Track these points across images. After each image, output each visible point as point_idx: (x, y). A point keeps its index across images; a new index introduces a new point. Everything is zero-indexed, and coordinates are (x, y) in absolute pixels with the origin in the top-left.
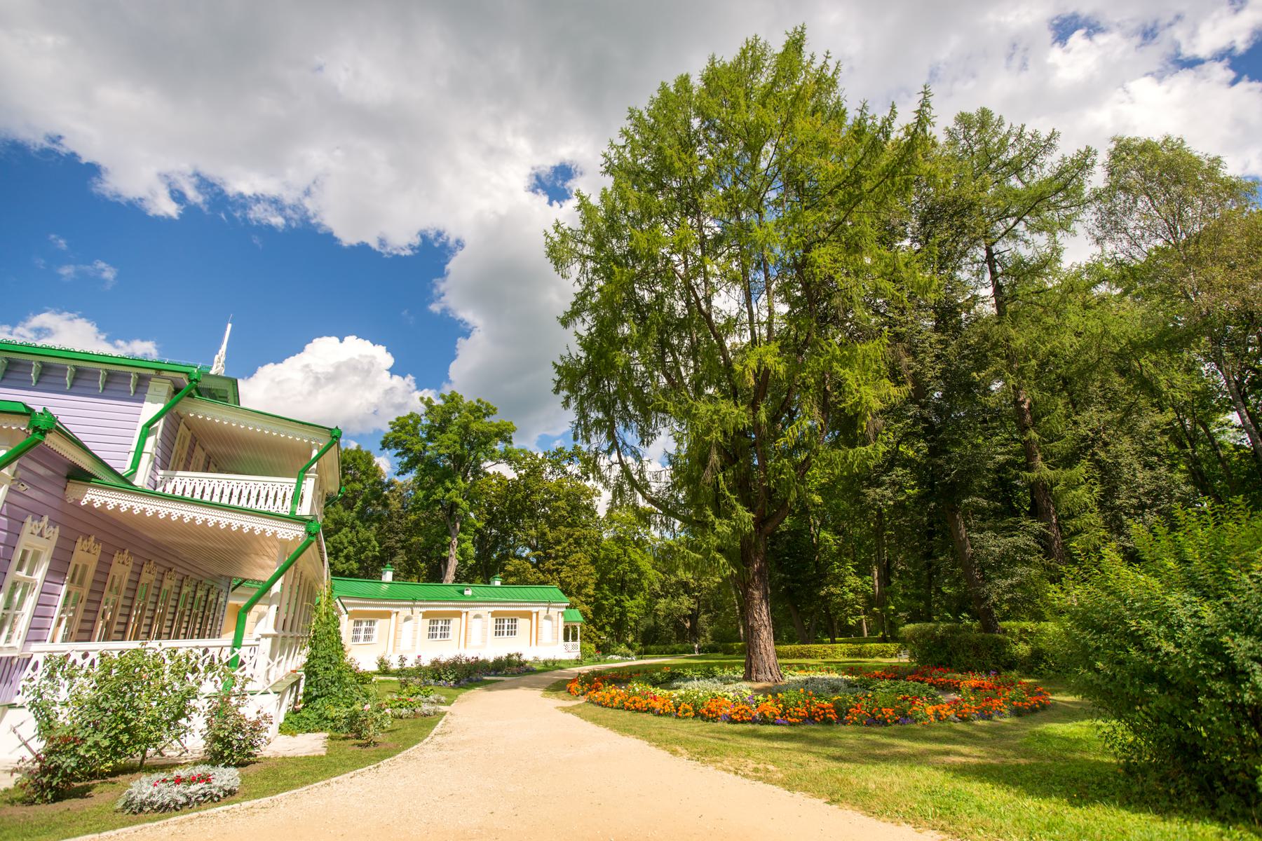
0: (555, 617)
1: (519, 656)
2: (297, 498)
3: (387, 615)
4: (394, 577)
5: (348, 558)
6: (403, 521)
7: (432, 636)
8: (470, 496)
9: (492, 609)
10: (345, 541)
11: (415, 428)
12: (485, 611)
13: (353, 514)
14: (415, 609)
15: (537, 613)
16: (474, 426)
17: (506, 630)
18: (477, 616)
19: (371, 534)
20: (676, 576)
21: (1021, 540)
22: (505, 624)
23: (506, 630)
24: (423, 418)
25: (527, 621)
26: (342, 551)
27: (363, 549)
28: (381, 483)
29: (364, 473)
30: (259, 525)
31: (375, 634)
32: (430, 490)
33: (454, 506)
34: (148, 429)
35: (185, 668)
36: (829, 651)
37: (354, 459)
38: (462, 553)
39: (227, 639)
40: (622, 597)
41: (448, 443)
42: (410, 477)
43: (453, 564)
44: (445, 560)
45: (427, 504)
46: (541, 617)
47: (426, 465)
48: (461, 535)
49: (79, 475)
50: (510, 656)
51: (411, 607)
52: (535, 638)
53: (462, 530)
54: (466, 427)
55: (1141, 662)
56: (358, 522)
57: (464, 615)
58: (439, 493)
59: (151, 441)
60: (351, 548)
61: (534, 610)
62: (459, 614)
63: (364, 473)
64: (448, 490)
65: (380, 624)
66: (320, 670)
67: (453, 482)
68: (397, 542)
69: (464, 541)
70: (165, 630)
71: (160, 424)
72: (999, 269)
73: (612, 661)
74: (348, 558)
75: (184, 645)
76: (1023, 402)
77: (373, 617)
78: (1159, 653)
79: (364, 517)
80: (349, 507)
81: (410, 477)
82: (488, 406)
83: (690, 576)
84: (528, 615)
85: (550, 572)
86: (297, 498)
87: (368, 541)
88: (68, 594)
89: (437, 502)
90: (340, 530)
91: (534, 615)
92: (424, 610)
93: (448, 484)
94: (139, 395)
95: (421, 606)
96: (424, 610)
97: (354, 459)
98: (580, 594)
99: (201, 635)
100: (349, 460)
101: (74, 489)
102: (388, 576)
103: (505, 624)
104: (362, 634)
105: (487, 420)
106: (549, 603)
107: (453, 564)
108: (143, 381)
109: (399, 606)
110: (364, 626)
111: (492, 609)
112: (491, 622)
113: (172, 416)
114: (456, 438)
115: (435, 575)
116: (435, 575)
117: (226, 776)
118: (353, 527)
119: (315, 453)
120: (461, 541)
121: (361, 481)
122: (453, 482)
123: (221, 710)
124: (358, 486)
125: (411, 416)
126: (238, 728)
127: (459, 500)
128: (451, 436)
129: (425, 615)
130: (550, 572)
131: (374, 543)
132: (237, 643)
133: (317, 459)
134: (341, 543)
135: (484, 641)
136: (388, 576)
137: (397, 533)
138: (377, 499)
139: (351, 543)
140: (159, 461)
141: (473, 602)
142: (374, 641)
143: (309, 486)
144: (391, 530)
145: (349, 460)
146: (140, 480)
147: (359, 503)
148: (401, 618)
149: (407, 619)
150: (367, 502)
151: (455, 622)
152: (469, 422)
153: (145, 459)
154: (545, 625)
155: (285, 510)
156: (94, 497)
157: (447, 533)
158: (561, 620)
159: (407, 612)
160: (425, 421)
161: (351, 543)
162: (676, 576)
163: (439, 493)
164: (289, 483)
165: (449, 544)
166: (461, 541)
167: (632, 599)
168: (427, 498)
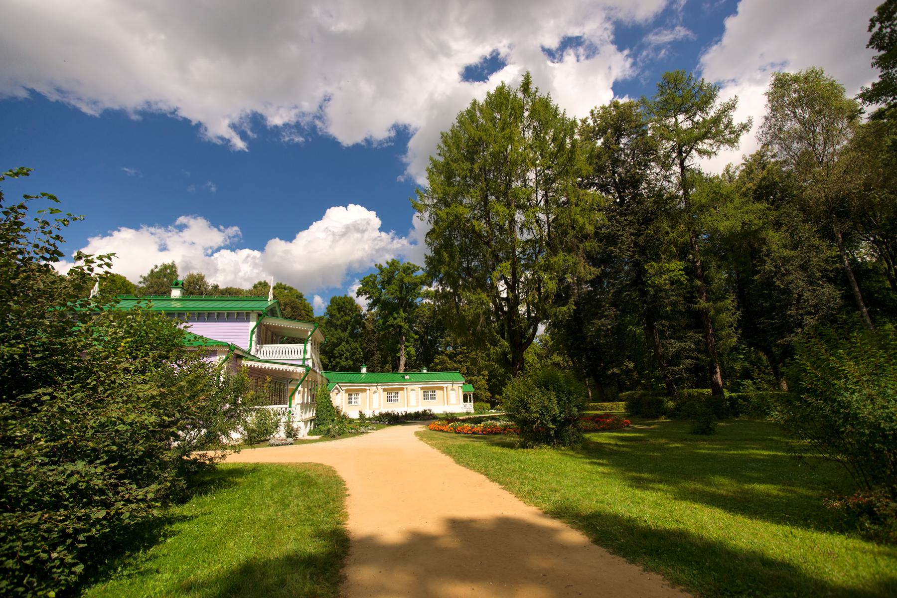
0: (457, 389)
1: (430, 411)
2: (305, 352)
3: (365, 390)
4: (367, 371)
5: (347, 359)
6: (377, 335)
7: (350, 403)
8: (410, 321)
9: (421, 386)
10: (344, 349)
11: (374, 283)
12: (417, 387)
13: (347, 334)
16: (406, 280)
18: (412, 390)
19: (357, 345)
20: (551, 359)
21: (689, 344)
22: (429, 394)
24: (378, 276)
25: (442, 391)
27: (353, 354)
28: (360, 315)
29: (350, 310)
30: (291, 368)
31: (359, 400)
32: (385, 318)
33: (401, 327)
34: (253, 332)
35: (277, 414)
36: (615, 406)
37: (344, 303)
38: (408, 354)
39: (287, 406)
41: (392, 291)
42: (375, 310)
43: (402, 363)
44: (399, 358)
45: (385, 326)
46: (449, 389)
47: (382, 304)
48: (406, 343)
50: (425, 411)
51: (376, 386)
52: (413, 402)
53: (407, 340)
54: (402, 280)
56: (350, 339)
58: (391, 321)
59: (254, 336)
60: (348, 353)
61: (445, 385)
62: (402, 389)
63: (350, 310)
64: (395, 319)
65: (361, 395)
66: (319, 415)
67: (398, 313)
68: (374, 347)
69: (408, 347)
71: (256, 330)
73: (491, 413)
74: (347, 359)
75: (276, 407)
76: (697, 262)
77: (357, 392)
79: (353, 335)
80: (344, 330)
81: (375, 310)
82: (414, 266)
83: (560, 359)
84: (442, 388)
85: (460, 362)
86: (305, 352)
87: (356, 349)
89: (390, 326)
90: (341, 344)
92: (383, 387)
93: (395, 315)
94: (248, 320)
96: (383, 387)
97: (344, 303)
98: (480, 374)
99: (280, 404)
100: (341, 303)
101: (238, 360)
102: (364, 370)
103: (429, 394)
104: (353, 400)
105: (414, 275)
106: (453, 382)
107: (402, 363)
108: (248, 314)
110: (353, 396)
111: (421, 386)
112: (421, 393)
113: (259, 326)
114: (396, 288)
115: (395, 368)
116: (395, 368)
117: (290, 440)
118: (347, 342)
119: (310, 333)
120: (406, 347)
121: (349, 315)
122: (398, 313)
123: (288, 425)
124: (348, 318)
125: (371, 276)
126: (292, 429)
127: (402, 324)
128: (394, 287)
129: (384, 390)
130: (460, 362)
131: (360, 350)
132: (290, 407)
133: (311, 335)
134: (342, 351)
135: (418, 402)
136: (364, 370)
137: (374, 342)
138: (359, 324)
139: (347, 350)
141: (410, 382)
142: (360, 403)
143: (309, 346)
144: (370, 340)
145: (341, 303)
146: (253, 352)
147: (349, 327)
148: (372, 392)
149: (375, 392)
150: (354, 328)
151: (400, 393)
152: (403, 278)
153: (253, 343)
154: (452, 394)
155: (301, 363)
157: (398, 342)
158: (461, 391)
160: (380, 278)
161: (347, 350)
162: (551, 359)
163: (391, 321)
164: (300, 346)
165: (400, 349)
166: (406, 347)
168: (384, 323)
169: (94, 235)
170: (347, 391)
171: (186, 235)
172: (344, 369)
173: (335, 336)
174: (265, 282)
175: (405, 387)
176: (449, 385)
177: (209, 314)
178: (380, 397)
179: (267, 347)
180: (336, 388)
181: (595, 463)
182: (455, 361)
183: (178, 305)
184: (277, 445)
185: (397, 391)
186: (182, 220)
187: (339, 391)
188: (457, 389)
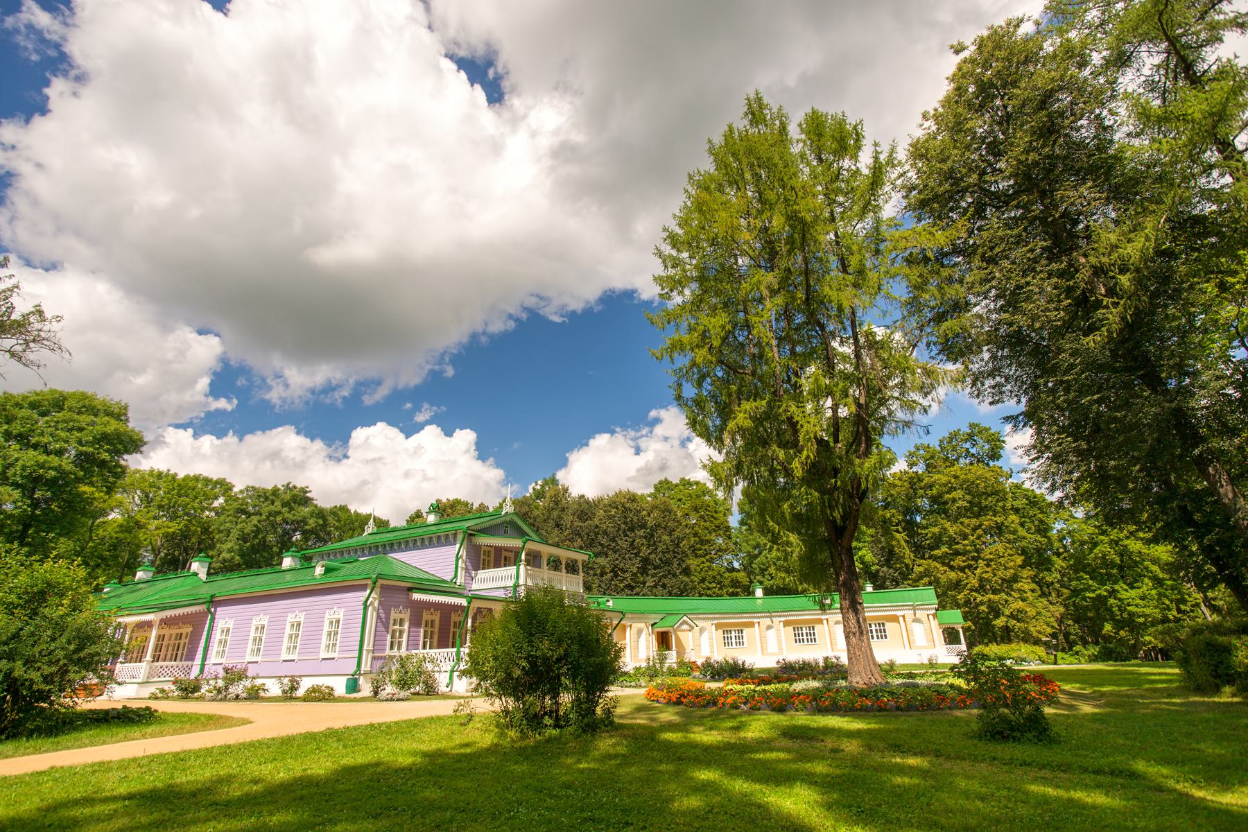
3: (751, 625)
14: (774, 619)
15: (903, 617)
17: (734, 641)
22: (732, 633)
23: (734, 641)
26: (766, 570)
40: (1116, 587)
49: (410, 589)
51: (771, 617)
55: (1110, 337)
57: (825, 622)
61: (899, 613)
70: (169, 656)
72: (862, 340)
78: (990, 400)
84: (895, 619)
85: (962, 569)
88: (425, 632)
91: (901, 619)
95: (779, 616)
96: (783, 619)
102: (759, 592)
109: (759, 617)
136: (759, 592)
140: (470, 568)
143: (522, 568)
148: (763, 627)
149: (769, 628)
154: (917, 629)
156: (417, 596)
159: (768, 622)
164: (511, 570)
167: (1132, 588)
169: (571, 450)
170: (718, 626)
171: (659, 430)
172: (676, 595)
173: (750, 543)
174: (666, 479)
175: (755, 620)
176: (909, 614)
177: (392, 545)
178: (779, 636)
179: (482, 574)
180: (685, 622)
181: (467, 745)
182: (952, 568)
183: (371, 539)
184: (398, 700)
185: (740, 628)
186: (653, 414)
187: (692, 628)
188: (925, 619)
